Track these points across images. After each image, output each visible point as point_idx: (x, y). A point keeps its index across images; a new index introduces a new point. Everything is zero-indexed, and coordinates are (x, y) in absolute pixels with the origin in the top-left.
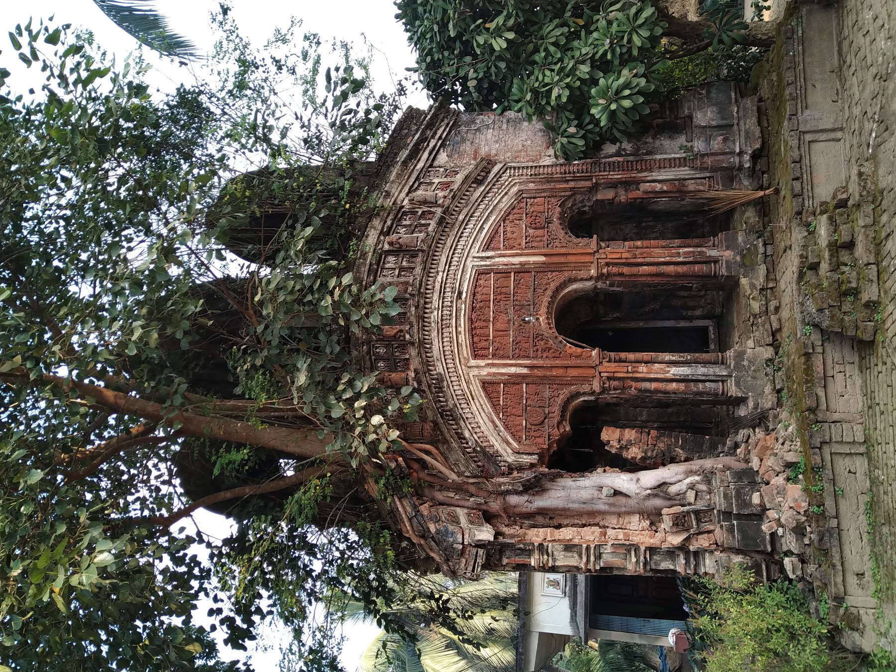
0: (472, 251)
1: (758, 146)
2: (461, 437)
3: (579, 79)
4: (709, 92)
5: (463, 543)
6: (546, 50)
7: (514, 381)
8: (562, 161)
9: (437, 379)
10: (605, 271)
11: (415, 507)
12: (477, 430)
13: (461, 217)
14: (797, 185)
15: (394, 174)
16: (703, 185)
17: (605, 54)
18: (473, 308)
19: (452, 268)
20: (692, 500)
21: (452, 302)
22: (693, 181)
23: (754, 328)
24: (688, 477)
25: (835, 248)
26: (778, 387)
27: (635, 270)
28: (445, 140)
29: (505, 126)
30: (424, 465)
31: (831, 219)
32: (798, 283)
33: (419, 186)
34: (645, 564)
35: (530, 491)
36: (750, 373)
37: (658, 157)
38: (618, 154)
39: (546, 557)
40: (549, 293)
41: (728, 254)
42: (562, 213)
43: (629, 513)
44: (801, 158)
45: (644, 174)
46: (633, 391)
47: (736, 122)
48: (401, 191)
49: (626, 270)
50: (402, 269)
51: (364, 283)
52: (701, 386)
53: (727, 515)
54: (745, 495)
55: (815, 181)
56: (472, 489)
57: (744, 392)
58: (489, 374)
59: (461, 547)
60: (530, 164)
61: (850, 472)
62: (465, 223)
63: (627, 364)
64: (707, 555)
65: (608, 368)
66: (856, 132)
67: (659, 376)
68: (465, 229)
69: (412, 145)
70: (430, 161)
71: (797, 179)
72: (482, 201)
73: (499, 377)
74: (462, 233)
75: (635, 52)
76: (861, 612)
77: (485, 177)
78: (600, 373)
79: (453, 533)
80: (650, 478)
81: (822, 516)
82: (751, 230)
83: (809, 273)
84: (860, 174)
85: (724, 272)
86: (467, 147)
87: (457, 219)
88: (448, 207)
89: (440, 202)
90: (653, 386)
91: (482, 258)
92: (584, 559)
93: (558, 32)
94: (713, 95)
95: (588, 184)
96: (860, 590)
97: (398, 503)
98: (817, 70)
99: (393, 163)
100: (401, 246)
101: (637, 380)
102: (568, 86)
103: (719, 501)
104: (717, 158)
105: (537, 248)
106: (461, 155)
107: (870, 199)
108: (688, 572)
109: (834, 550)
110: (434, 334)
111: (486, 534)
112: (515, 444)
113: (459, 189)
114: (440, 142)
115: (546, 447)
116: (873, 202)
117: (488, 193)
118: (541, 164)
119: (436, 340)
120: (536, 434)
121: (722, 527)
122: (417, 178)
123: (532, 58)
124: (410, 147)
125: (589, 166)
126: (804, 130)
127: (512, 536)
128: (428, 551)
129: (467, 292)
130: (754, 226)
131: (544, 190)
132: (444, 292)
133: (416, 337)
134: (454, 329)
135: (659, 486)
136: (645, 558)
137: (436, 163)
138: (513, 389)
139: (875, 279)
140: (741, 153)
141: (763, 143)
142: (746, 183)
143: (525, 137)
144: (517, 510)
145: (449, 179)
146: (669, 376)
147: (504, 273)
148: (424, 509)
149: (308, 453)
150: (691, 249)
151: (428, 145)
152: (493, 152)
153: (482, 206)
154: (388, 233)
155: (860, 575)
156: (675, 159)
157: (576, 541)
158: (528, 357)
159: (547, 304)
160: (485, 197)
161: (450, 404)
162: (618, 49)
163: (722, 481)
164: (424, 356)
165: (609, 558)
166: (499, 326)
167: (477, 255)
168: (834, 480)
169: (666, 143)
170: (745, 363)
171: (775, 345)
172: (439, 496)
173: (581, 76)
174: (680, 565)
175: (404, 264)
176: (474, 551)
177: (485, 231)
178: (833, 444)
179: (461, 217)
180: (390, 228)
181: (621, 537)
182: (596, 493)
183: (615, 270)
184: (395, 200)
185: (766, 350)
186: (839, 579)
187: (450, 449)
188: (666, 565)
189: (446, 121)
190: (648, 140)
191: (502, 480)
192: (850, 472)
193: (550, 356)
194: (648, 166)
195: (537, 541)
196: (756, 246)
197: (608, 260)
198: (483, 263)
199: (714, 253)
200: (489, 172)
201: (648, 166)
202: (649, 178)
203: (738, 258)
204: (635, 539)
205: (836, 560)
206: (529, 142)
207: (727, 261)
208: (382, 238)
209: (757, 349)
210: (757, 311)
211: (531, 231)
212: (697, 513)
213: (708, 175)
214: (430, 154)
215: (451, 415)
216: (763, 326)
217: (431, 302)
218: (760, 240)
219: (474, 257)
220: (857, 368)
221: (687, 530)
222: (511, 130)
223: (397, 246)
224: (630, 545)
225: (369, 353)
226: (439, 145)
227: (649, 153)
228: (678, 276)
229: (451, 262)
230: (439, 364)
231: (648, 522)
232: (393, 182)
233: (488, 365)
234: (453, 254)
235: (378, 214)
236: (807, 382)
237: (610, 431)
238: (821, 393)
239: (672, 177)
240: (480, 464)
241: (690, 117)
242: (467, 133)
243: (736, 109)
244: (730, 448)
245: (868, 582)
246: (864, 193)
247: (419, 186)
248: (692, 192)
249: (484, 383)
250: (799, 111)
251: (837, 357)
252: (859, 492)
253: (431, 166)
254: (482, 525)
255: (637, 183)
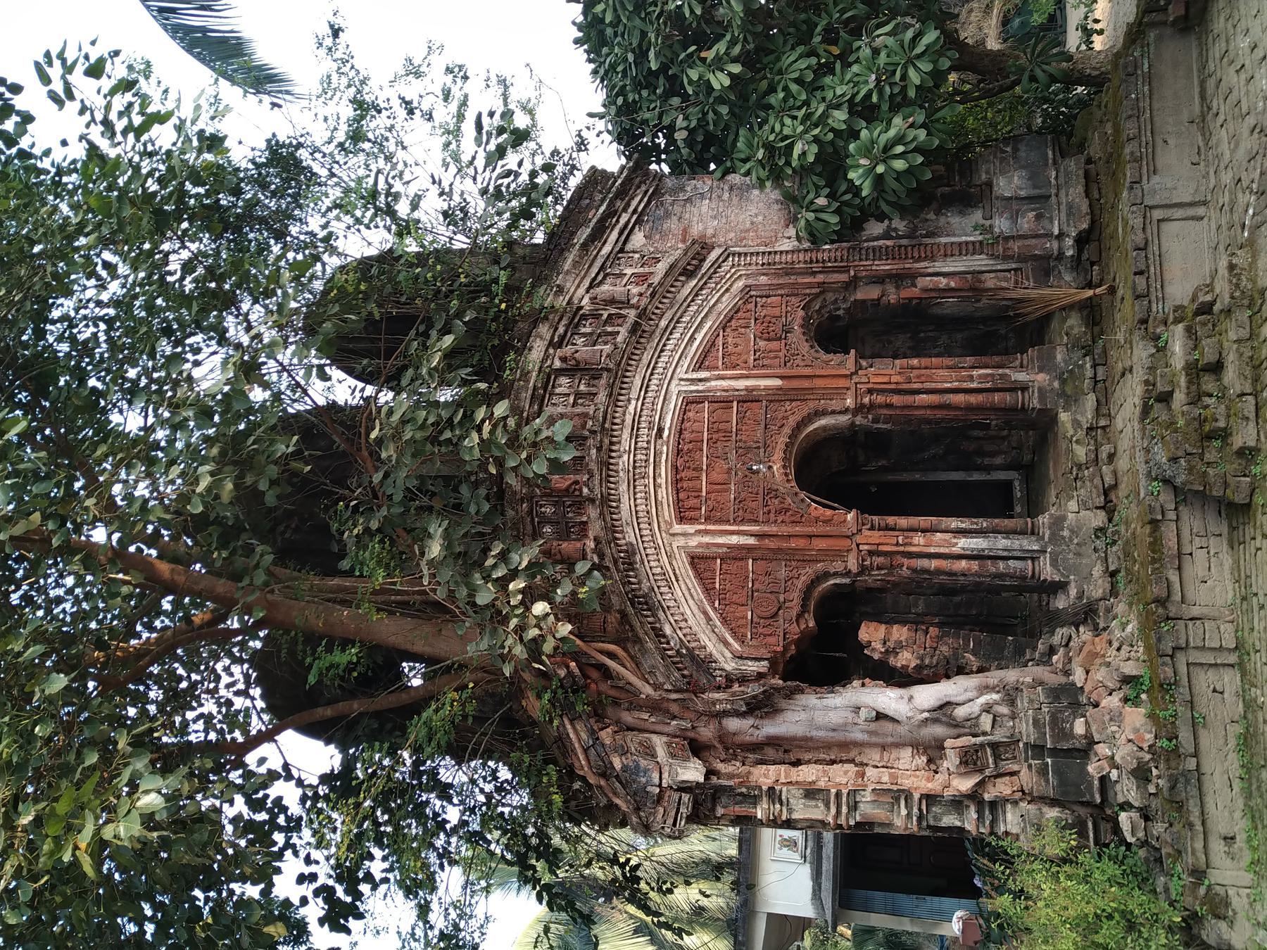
0: (678, 370)
1: (1085, 226)
2: (659, 634)
3: (832, 130)
4: (1015, 150)
5: (660, 786)
6: (786, 89)
7: (736, 555)
8: (806, 245)
9: (627, 551)
10: (866, 400)
11: (592, 733)
12: (683, 624)
13: (663, 323)
14: (1141, 282)
15: (569, 261)
16: (1006, 279)
17: (869, 95)
18: (679, 452)
19: (650, 394)
20: (988, 728)
21: (648, 442)
22: (992, 275)
23: (1079, 484)
24: (982, 694)
25: (1195, 371)
26: (1112, 568)
27: (908, 399)
28: (641, 214)
29: (726, 196)
30: (606, 673)
31: (1189, 330)
32: (1142, 420)
33: (604, 278)
34: (920, 818)
35: (757, 712)
36: (1072, 547)
37: (943, 240)
38: (886, 235)
39: (778, 806)
40: (787, 430)
41: (1042, 378)
42: (806, 319)
43: (898, 745)
44: (1146, 244)
45: (923, 264)
46: (905, 572)
47: (1053, 191)
48: (578, 286)
49: (896, 400)
50: (578, 395)
51: (525, 414)
52: (1001, 565)
53: (1038, 749)
54: (1063, 721)
55: (1167, 276)
56: (674, 708)
57: (1062, 575)
58: (700, 545)
59: (658, 790)
60: (762, 249)
61: (1215, 691)
62: (669, 330)
63: (897, 533)
64: (1009, 806)
65: (870, 538)
66: (1226, 207)
67: (942, 550)
68: (668, 339)
69: (595, 220)
70: (620, 244)
71: (1141, 273)
72: (693, 301)
73: (715, 549)
74: (665, 345)
75: (912, 93)
76: (1230, 892)
77: (698, 267)
78: (858, 545)
79: (646, 771)
80: (927, 695)
81: (1174, 754)
82: (1075, 345)
83: (1157, 406)
84: (1232, 267)
85: (1035, 403)
86: (673, 225)
87: (657, 325)
88: (645, 309)
89: (634, 301)
90: (934, 564)
91: (693, 381)
92: (833, 810)
93: (802, 64)
94: (1022, 154)
95: (843, 277)
96: (1229, 861)
97: (569, 727)
98: (1170, 120)
99: (569, 245)
100: (578, 363)
101: (910, 555)
102: (816, 140)
103: (1026, 730)
104: (1027, 242)
105: (770, 366)
106: (664, 236)
107: (1246, 302)
108: (982, 830)
109: (1191, 802)
110: (623, 487)
111: (693, 772)
112: (736, 646)
113: (661, 284)
114: (635, 217)
115: (779, 649)
116: (1249, 307)
117: (701, 289)
118: (777, 249)
119: (626, 496)
120: (765, 631)
121: (1030, 766)
122: (602, 268)
123: (765, 101)
124: (592, 225)
125: (845, 252)
126: (1150, 203)
127: (731, 776)
128: (611, 795)
129: (670, 429)
130: (1080, 338)
131: (781, 286)
132: (638, 429)
133: (597, 491)
134: (651, 481)
135: (941, 707)
136: (920, 809)
137: (629, 247)
138: (733, 567)
139: (1252, 416)
140: (1061, 236)
141: (1093, 222)
142: (1068, 277)
143: (754, 211)
144: (738, 739)
145: (647, 270)
146: (956, 550)
147: (723, 402)
148: (606, 736)
149: (443, 654)
150: (989, 371)
151: (618, 221)
152: (710, 232)
153: (693, 308)
154: (559, 345)
155: (1229, 839)
156: (967, 243)
157: (822, 784)
158: (755, 522)
159: (783, 447)
160: (697, 295)
161: (645, 586)
162: (887, 89)
163: (1031, 701)
164: (608, 519)
165: (868, 809)
166: (715, 476)
167: (686, 376)
168: (1192, 702)
169: (955, 220)
170: (1066, 533)
171: (1109, 508)
172: (628, 718)
173: (835, 125)
174: (970, 821)
175: (582, 387)
176: (676, 796)
177: (697, 343)
178: (1191, 651)
179: (663, 323)
180: (563, 337)
181: (885, 779)
182: (850, 716)
183: (880, 399)
184: (571, 299)
185: (1096, 515)
186: (1199, 845)
187: (644, 651)
188: (950, 820)
189: (644, 188)
190: (928, 217)
191: (717, 696)
192: (1215, 691)
193: (787, 520)
194: (929, 253)
195: (765, 783)
196: (1082, 367)
197: (870, 386)
198: (693, 388)
199: (1021, 376)
200: (704, 260)
201: (929, 253)
202: (930, 270)
203: (1056, 384)
204: (907, 783)
205: (1195, 818)
206: (760, 218)
207: (1040, 389)
208: (551, 351)
209: (1083, 513)
210: (1083, 459)
211: (762, 344)
212: (995, 746)
213: (1014, 266)
214: (621, 234)
215: (646, 603)
216: (1091, 481)
217: (620, 442)
218: (1087, 358)
219: (681, 380)
220: (1225, 543)
221: (981, 771)
222: (735, 200)
223: (573, 362)
224: (899, 791)
225: (530, 512)
226: (633, 221)
227: (931, 235)
228: (969, 408)
229: (648, 386)
230: (630, 530)
231: (924, 759)
232: (568, 272)
233: (699, 532)
234: (652, 374)
235: (546, 318)
236: (1154, 561)
237: (872, 629)
238: (1174, 578)
239: (963, 269)
240: (685, 672)
241: (989, 184)
242: (672, 204)
243: (1054, 174)
244: (1042, 655)
245: (1241, 849)
246: (1237, 294)
247: (604, 278)
248: (990, 290)
249: (692, 558)
250: (1145, 178)
251: (1197, 525)
252: (1227, 721)
253: (622, 250)
254: (687, 759)
255: (913, 276)
